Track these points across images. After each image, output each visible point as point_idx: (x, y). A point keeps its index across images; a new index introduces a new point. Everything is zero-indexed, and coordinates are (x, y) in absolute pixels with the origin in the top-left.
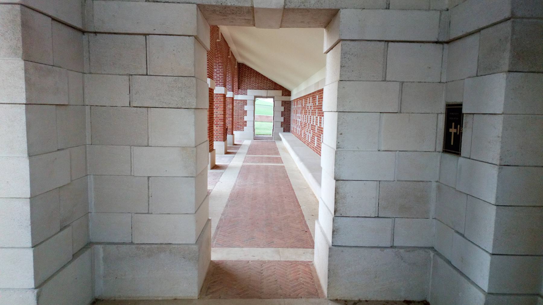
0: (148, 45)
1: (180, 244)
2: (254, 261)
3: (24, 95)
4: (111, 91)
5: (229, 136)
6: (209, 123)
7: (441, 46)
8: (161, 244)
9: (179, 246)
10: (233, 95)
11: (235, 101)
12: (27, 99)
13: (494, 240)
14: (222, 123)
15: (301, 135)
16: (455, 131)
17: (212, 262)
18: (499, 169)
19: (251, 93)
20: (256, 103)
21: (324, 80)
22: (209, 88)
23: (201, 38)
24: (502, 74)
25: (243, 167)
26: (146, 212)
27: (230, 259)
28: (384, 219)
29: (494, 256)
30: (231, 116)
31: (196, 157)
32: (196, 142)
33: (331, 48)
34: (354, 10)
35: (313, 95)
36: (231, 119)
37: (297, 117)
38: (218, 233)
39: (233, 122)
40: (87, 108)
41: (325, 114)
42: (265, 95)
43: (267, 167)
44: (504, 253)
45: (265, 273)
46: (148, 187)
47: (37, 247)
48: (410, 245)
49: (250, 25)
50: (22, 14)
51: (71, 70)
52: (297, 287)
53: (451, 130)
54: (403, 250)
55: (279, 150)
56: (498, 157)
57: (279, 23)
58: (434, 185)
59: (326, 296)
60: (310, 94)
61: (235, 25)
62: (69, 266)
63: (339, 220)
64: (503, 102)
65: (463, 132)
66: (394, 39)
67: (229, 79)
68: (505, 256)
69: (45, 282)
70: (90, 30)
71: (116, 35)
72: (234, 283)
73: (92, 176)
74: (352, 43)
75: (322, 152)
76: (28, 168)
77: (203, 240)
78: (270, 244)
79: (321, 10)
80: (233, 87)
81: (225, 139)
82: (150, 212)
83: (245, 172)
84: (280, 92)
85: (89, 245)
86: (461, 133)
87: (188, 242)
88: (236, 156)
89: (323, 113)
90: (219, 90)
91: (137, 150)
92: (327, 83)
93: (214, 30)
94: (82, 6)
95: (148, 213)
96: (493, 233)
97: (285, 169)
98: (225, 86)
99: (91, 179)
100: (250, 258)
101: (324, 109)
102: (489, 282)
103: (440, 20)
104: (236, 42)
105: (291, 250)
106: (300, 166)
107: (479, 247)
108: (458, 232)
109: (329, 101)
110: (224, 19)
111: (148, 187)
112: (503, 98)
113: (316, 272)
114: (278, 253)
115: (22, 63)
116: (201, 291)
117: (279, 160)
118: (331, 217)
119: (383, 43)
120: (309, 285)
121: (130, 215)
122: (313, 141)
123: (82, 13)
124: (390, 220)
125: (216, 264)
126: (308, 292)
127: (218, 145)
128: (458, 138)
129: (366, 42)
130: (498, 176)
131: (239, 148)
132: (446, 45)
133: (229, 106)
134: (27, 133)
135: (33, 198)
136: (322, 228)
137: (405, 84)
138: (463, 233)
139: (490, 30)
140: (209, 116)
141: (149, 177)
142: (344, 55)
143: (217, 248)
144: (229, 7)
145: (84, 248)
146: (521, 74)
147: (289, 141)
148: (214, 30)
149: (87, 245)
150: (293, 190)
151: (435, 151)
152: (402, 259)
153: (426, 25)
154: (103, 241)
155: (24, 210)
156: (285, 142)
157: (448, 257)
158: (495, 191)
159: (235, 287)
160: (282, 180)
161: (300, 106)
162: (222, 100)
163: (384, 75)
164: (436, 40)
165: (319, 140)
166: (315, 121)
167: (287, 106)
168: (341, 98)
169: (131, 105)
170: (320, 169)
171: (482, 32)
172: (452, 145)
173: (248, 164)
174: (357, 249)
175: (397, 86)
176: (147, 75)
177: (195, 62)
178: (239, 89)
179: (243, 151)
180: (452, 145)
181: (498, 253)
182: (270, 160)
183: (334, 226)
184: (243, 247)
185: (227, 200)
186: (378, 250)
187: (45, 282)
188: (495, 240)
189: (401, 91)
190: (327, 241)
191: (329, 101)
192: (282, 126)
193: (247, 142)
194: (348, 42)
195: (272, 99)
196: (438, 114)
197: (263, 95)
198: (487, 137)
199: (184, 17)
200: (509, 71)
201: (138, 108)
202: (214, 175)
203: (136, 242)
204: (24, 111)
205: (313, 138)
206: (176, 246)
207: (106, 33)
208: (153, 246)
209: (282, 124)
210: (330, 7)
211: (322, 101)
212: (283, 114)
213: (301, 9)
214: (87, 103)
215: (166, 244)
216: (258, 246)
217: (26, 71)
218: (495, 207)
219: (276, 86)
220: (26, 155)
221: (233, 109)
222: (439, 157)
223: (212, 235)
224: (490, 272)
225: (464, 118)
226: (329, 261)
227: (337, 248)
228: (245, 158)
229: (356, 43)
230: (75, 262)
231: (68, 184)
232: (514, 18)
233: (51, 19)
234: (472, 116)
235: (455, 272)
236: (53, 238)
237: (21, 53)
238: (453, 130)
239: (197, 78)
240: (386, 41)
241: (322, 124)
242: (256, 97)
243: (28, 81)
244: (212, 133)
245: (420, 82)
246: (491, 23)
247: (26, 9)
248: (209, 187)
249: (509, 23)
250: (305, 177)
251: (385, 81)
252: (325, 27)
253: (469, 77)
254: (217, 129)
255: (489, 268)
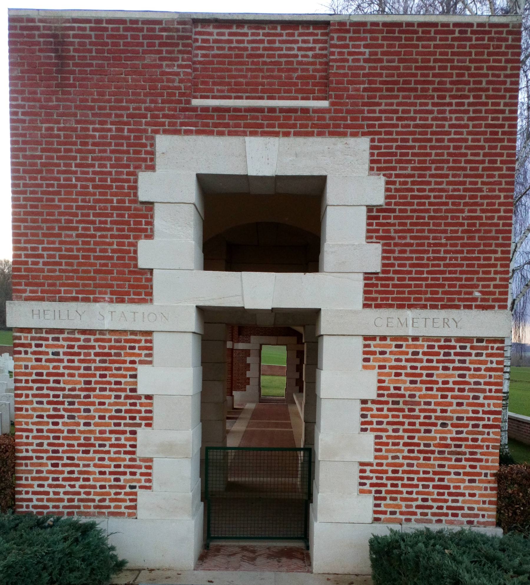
25: (246, 432)
88: (238, 421)
117: (289, 425)
182: (277, 425)
193: (251, 406)
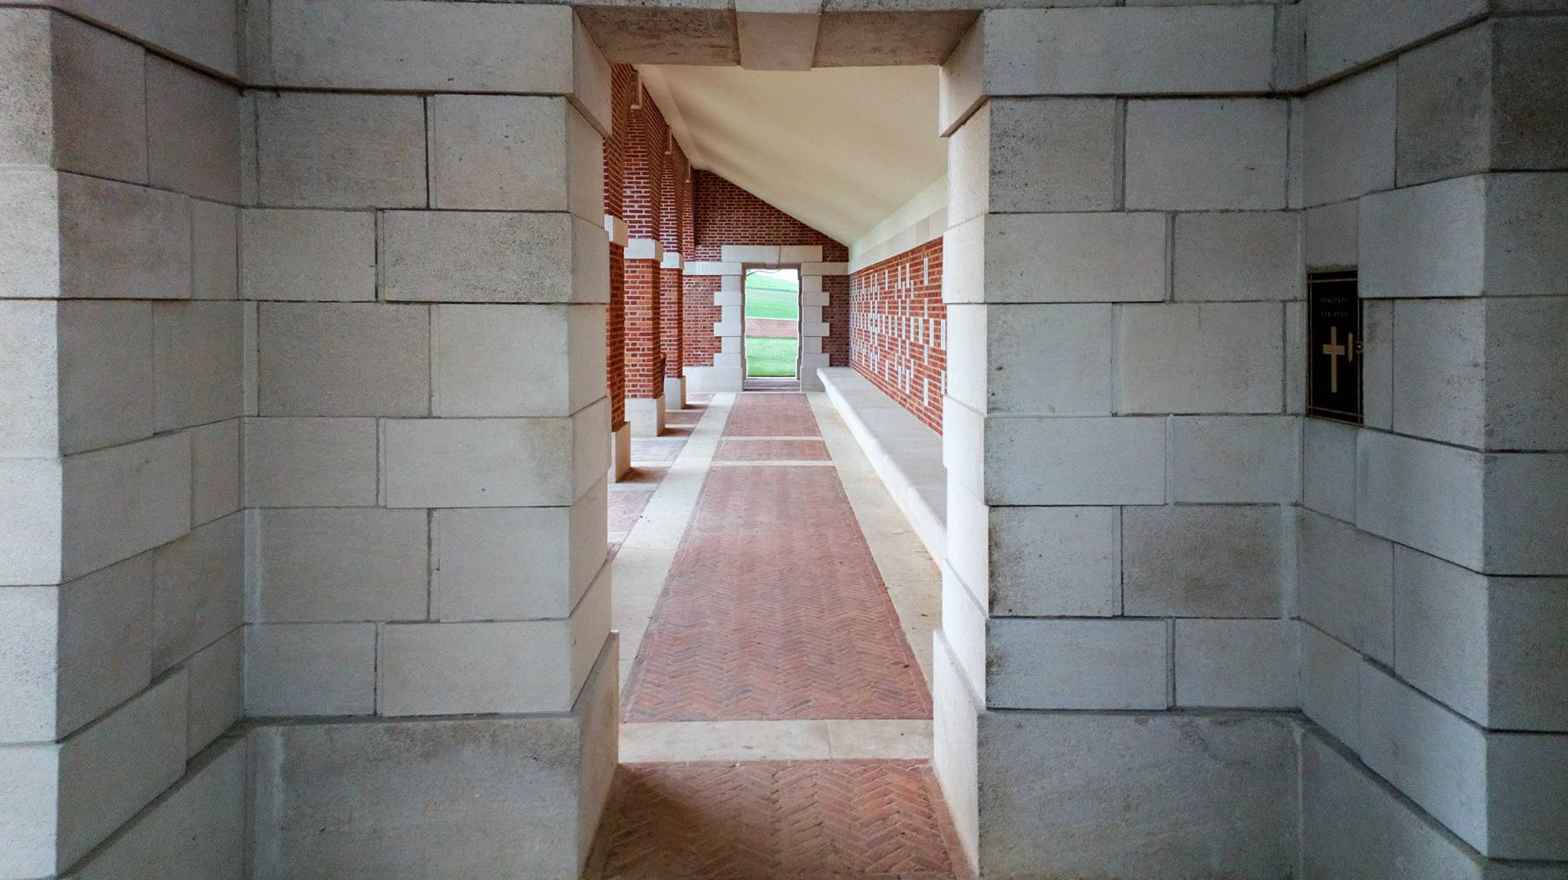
0: (430, 124)
1: (523, 716)
2: (750, 763)
3: (55, 274)
4: (319, 258)
5: (670, 383)
6: (612, 344)
7: (1283, 104)
8: (467, 716)
9: (520, 721)
10: (681, 263)
11: (685, 280)
12: (63, 284)
13: (1490, 684)
14: (650, 345)
15: (882, 373)
16: (1340, 350)
17: (621, 769)
18: (1486, 461)
19: (732, 256)
20: (747, 284)
21: (943, 213)
22: (611, 244)
23: (586, 102)
24: (1471, 179)
25: (711, 473)
26: (422, 617)
27: (677, 759)
28: (1141, 623)
29: (1496, 737)
30: (674, 324)
31: (574, 444)
32: (572, 400)
33: (962, 122)
34: (1023, 11)
35: (913, 256)
36: (675, 332)
37: (867, 323)
38: (641, 676)
39: (680, 341)
40: (249, 309)
41: (950, 310)
42: (775, 261)
43: (782, 474)
44: (1528, 728)
45: (785, 803)
46: (430, 545)
47: (75, 741)
48: (1227, 705)
49: (727, 62)
50: (55, 36)
51: (202, 199)
52: (886, 845)
53: (1327, 349)
54: (1207, 720)
56: (1480, 425)
57: (811, 55)
58: (1288, 514)
59: (977, 871)
60: (906, 254)
61: (683, 63)
62: (174, 800)
63: (1006, 627)
64: (1481, 261)
65: (1366, 354)
66: (1143, 90)
67: (667, 216)
68: (1533, 738)
69: (93, 853)
70: (261, 83)
71: (338, 96)
72: (690, 835)
73: (257, 511)
74: (1021, 106)
75: (945, 422)
76: (60, 493)
77: (594, 702)
78: (797, 708)
79: (929, 13)
80: (680, 239)
81: (658, 392)
82: (433, 617)
83: (718, 487)
84: (816, 251)
85: (241, 726)
86: (1359, 358)
87: (547, 709)
88: (691, 439)
89: (944, 308)
90: (639, 248)
91: (395, 430)
92: (952, 221)
93: (624, 79)
94: (237, 12)
95: (427, 621)
96: (1486, 661)
97: (836, 477)
98: (656, 236)
99: (254, 522)
100: (737, 752)
101: (947, 296)
102: (1490, 822)
103: (1275, 30)
104: (686, 111)
105: (863, 724)
106: (881, 466)
107: (1447, 707)
108: (1372, 661)
109: (961, 274)
110: (652, 46)
111: (430, 545)
112: (1480, 250)
113: (941, 795)
114: (824, 734)
115: (52, 178)
116: (587, 865)
117: (820, 450)
118: (979, 618)
119: (1112, 102)
120: (922, 837)
121: (372, 627)
122: (917, 392)
123: (239, 34)
124: (1161, 624)
125: (635, 777)
126: (919, 860)
127: (640, 411)
128: (1352, 371)
129: (1063, 101)
130: (1486, 484)
131: (701, 415)
132: (1296, 103)
133: (669, 296)
134: (62, 383)
135: (67, 585)
136: (954, 652)
137: (1182, 217)
138: (1390, 664)
139: (1427, 52)
140: (612, 324)
141: (430, 511)
142: (998, 140)
143: (635, 725)
144: (665, 12)
145: (224, 736)
146: (1532, 176)
147: (845, 394)
148: (624, 79)
149: (233, 728)
150: (862, 538)
151: (1284, 412)
152: (1206, 749)
153: (1237, 45)
154: (283, 713)
155: (41, 620)
156: (837, 397)
157: (1350, 739)
158: (1479, 530)
159: (694, 849)
160: (829, 508)
161: (876, 289)
162: (649, 277)
163: (1119, 193)
164: (1266, 89)
165: (935, 388)
166: (921, 331)
167: (838, 290)
168: (995, 264)
169: (381, 297)
170: (941, 475)
171: (1403, 59)
172: (1335, 393)
173: (728, 463)
174: (1065, 719)
175: (1159, 224)
176: (428, 208)
177: (568, 168)
178: (697, 243)
179: (712, 425)
180: (1335, 393)
181: (1507, 727)
182: (790, 450)
183: (989, 649)
184: (715, 720)
185: (665, 574)
186: (1130, 720)
187: (93, 853)
188: (1496, 685)
189: (1172, 238)
190: (971, 693)
191: (961, 274)
193: (724, 400)
194: (1010, 104)
196: (1284, 302)
197: (768, 261)
198: (1446, 365)
199: (542, 44)
200: (1493, 171)
201: (401, 307)
202: (627, 499)
203: (387, 714)
204: (54, 320)
205: (917, 381)
206: (512, 722)
207: (306, 90)
208: (440, 723)
209: (826, 344)
210: (955, 6)
211: (940, 273)
212: (827, 315)
213: (870, 13)
214: (248, 293)
215: (480, 716)
216: (762, 714)
217: (64, 201)
218: (1484, 581)
219: (804, 234)
220: (54, 452)
221: (680, 302)
222: (1297, 430)
223: (621, 685)
224: (1490, 790)
225: (1365, 313)
226: (980, 758)
227: (1001, 717)
228: (718, 446)
229: (1032, 104)
230: (196, 781)
231: (183, 538)
232: (1498, 16)
233: (142, 51)
234: (1388, 304)
235: (1374, 788)
236: (125, 710)
237: (50, 148)
238: (1333, 350)
239: (574, 216)
240: (1119, 97)
241: (943, 342)
242: (746, 266)
243: (68, 230)
244: (621, 374)
245: (1227, 211)
246: (1428, 32)
247: (68, 21)
248: (613, 537)
249: (1484, 30)
250: (897, 500)
251: (1122, 209)
252: (942, 64)
253: (1373, 192)
254: (635, 363)
255: (1484, 776)
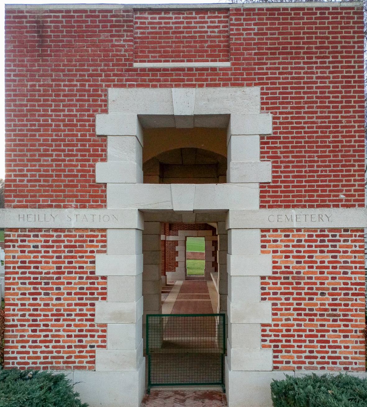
25: (176, 302)
43: (196, 302)
55: (209, 289)
88: (170, 294)
117: (208, 297)
178: (170, 229)
192: (263, 156)
193: (179, 283)
195: (204, 238)
197: (194, 235)
221: (165, 251)
